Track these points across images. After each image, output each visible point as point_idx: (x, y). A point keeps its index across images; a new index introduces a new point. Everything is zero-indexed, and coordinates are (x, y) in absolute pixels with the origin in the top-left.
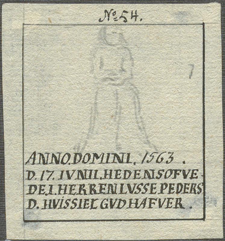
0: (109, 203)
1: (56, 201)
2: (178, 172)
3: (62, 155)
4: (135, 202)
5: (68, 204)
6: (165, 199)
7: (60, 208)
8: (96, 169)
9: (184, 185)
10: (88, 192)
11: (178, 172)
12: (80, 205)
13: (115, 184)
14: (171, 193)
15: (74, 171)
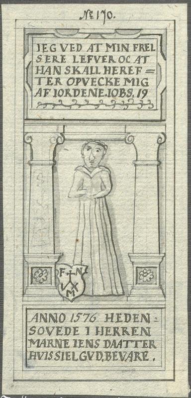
0: (86, 355)
1: (41, 354)
2: (91, 57)
3: (58, 316)
4: (110, 317)
5: (51, 356)
6: (126, 361)
7: (46, 359)
8: (37, 323)
9: (57, 95)
10: (121, 333)
11: (91, 57)
12: (63, 358)
13: (147, 314)
14: (59, 335)
15: (54, 327)
